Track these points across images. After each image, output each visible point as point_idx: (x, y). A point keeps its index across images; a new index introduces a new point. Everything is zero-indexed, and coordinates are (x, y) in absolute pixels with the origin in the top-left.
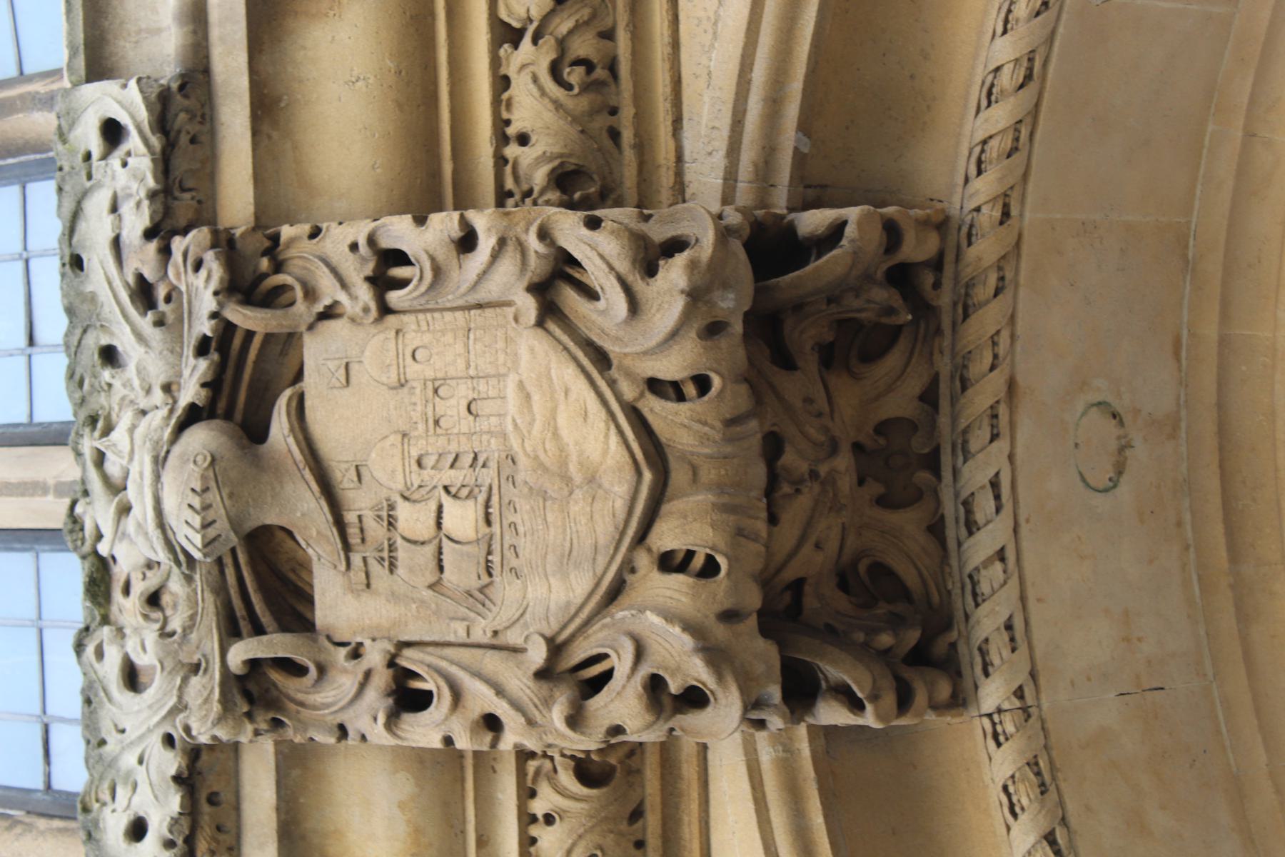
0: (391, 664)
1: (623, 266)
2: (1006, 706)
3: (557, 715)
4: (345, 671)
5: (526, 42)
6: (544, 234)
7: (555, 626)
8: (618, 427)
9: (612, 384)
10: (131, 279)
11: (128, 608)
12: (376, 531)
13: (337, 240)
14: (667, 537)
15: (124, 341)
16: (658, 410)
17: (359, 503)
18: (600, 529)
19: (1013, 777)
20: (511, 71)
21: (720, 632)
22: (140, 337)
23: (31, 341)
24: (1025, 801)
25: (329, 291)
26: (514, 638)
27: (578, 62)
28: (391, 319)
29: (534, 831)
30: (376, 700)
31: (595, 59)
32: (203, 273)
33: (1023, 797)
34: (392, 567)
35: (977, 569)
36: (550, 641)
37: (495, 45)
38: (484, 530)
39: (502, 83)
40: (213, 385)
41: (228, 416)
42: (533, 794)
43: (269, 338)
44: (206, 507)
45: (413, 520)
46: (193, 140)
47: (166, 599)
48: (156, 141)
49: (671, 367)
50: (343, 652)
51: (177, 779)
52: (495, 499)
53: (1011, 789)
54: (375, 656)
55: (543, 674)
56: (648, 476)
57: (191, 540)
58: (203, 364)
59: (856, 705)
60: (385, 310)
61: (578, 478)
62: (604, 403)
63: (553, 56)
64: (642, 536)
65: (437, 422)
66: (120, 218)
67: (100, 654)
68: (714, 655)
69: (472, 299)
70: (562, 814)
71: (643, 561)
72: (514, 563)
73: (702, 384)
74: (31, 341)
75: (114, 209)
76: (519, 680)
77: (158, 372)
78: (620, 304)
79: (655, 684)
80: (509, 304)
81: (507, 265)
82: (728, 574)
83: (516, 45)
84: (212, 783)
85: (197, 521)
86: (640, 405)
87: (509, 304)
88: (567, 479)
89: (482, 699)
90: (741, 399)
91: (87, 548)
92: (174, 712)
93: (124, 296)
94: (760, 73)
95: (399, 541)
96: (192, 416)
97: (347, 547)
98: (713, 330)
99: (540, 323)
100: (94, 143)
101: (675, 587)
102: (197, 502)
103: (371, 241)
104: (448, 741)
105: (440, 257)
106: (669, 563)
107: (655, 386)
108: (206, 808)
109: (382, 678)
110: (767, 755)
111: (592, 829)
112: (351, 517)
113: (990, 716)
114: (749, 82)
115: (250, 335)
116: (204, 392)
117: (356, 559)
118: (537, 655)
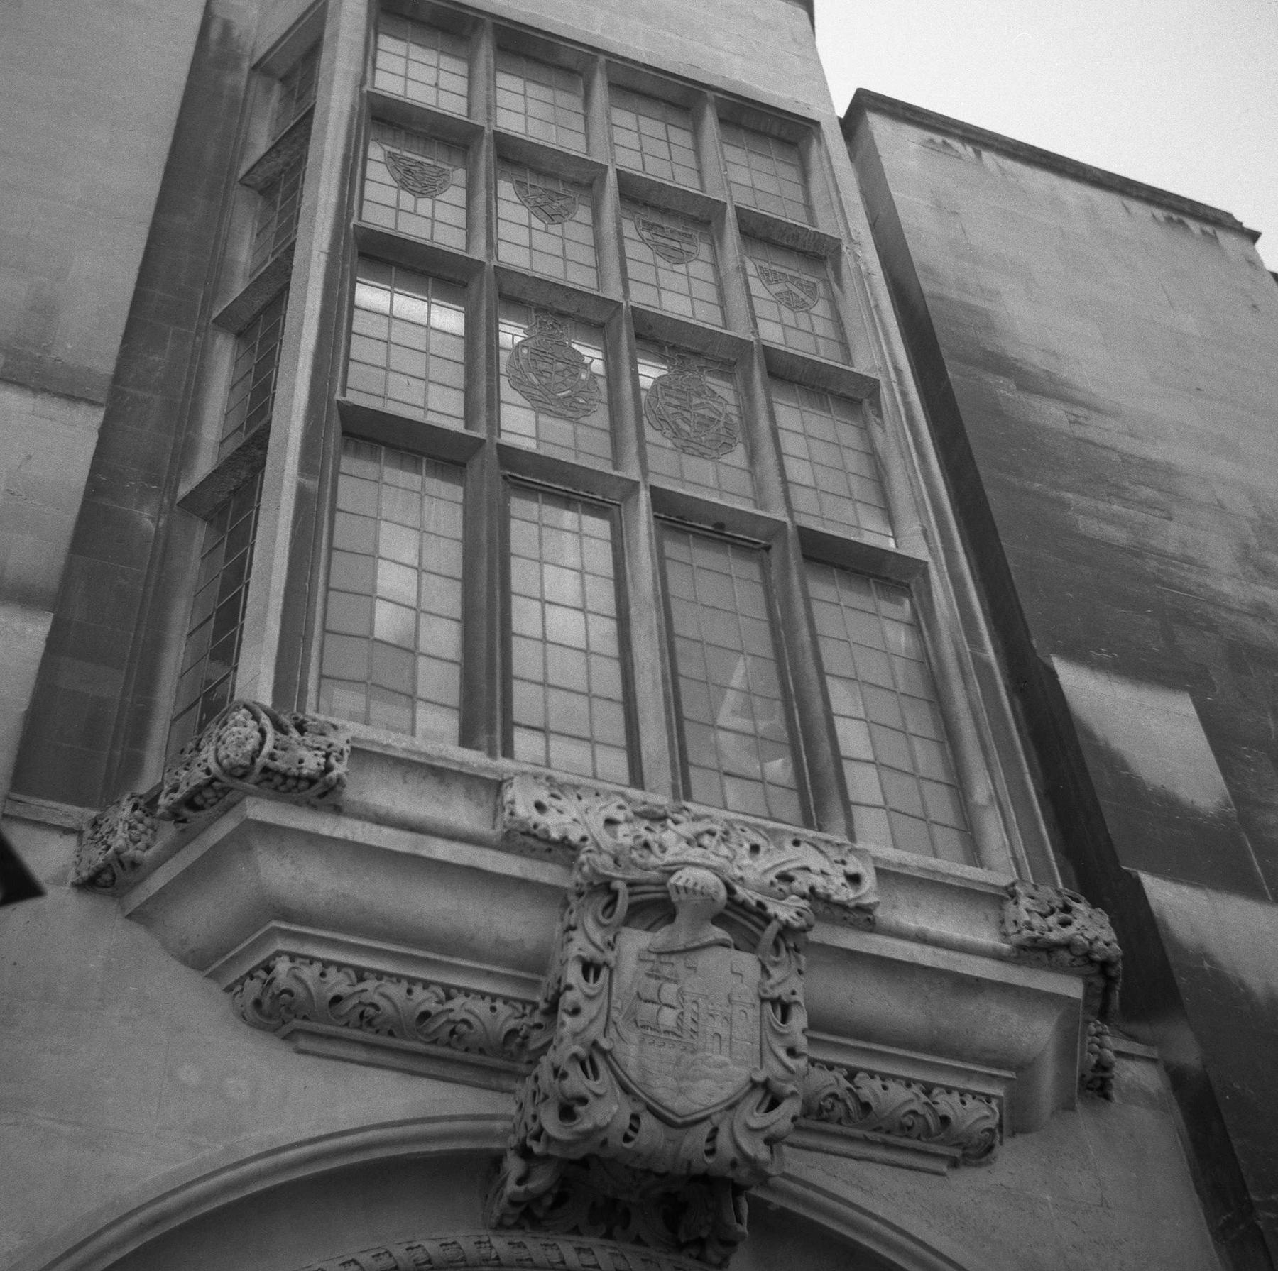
0: (606, 964)
1: (773, 1130)
2: (493, 1252)
3: (576, 1048)
4: (603, 938)
5: (848, 1085)
6: (793, 1094)
7: (618, 1056)
8: (702, 1111)
9: (721, 1111)
10: (791, 873)
11: (641, 827)
12: (666, 970)
13: (796, 983)
14: (647, 1121)
15: (763, 862)
16: (705, 1129)
17: (679, 964)
18: (660, 1091)
19: (460, 1248)
20: (835, 1073)
21: (601, 1137)
22: (766, 872)
23: (727, 774)
24: (448, 1252)
25: (777, 974)
26: (612, 1031)
27: (833, 1106)
28: (758, 1003)
29: (488, 999)
30: (589, 952)
31: (831, 1114)
32: (795, 916)
33: (450, 1252)
34: (648, 975)
35: (558, 1249)
36: (610, 1052)
37: (848, 1068)
38: (662, 1028)
39: (831, 1067)
40: (743, 905)
41: (727, 907)
42: (505, 1003)
43: (758, 938)
44: (694, 892)
45: (669, 991)
46: (845, 919)
47: (645, 852)
48: (852, 904)
49: (723, 1140)
50: (611, 938)
51: (565, 838)
52: (675, 1038)
53: (454, 1246)
54: (610, 956)
55: (595, 1044)
56: (679, 1120)
57: (680, 878)
58: (754, 903)
59: (520, 1181)
60: (763, 1000)
61: (684, 1084)
62: (714, 1106)
63: (840, 1096)
64: (650, 1109)
65: (711, 1015)
66: (818, 875)
67: (620, 807)
68: (588, 1135)
69: (766, 1047)
70: (495, 1018)
71: (639, 1107)
72: (647, 1041)
73: (711, 1152)
74: (727, 774)
75: (823, 873)
76: (595, 1032)
77: (750, 876)
78: (754, 1123)
79: (583, 1101)
80: (761, 1067)
81: (779, 1071)
82: (623, 1148)
83: (846, 1078)
84: (558, 852)
85: (690, 885)
86: (708, 1122)
87: (761, 1067)
88: (682, 1078)
89: (589, 1009)
90: (698, 1168)
91: (669, 813)
92: (597, 845)
93: (784, 868)
94: (811, 1194)
95: (661, 982)
96: (730, 891)
97: (659, 954)
98: (734, 1164)
99: (752, 1081)
100: (851, 869)
101: (625, 1121)
102: (698, 888)
103: (797, 1003)
104: (569, 987)
105: (789, 1038)
106: (635, 1117)
107: (715, 1130)
108: (546, 847)
109: (599, 958)
110: (498, 1125)
111: (485, 1029)
112: (673, 959)
113: (489, 1241)
114: (808, 1188)
115: (763, 929)
116: (740, 899)
117: (653, 957)
118: (605, 1044)
